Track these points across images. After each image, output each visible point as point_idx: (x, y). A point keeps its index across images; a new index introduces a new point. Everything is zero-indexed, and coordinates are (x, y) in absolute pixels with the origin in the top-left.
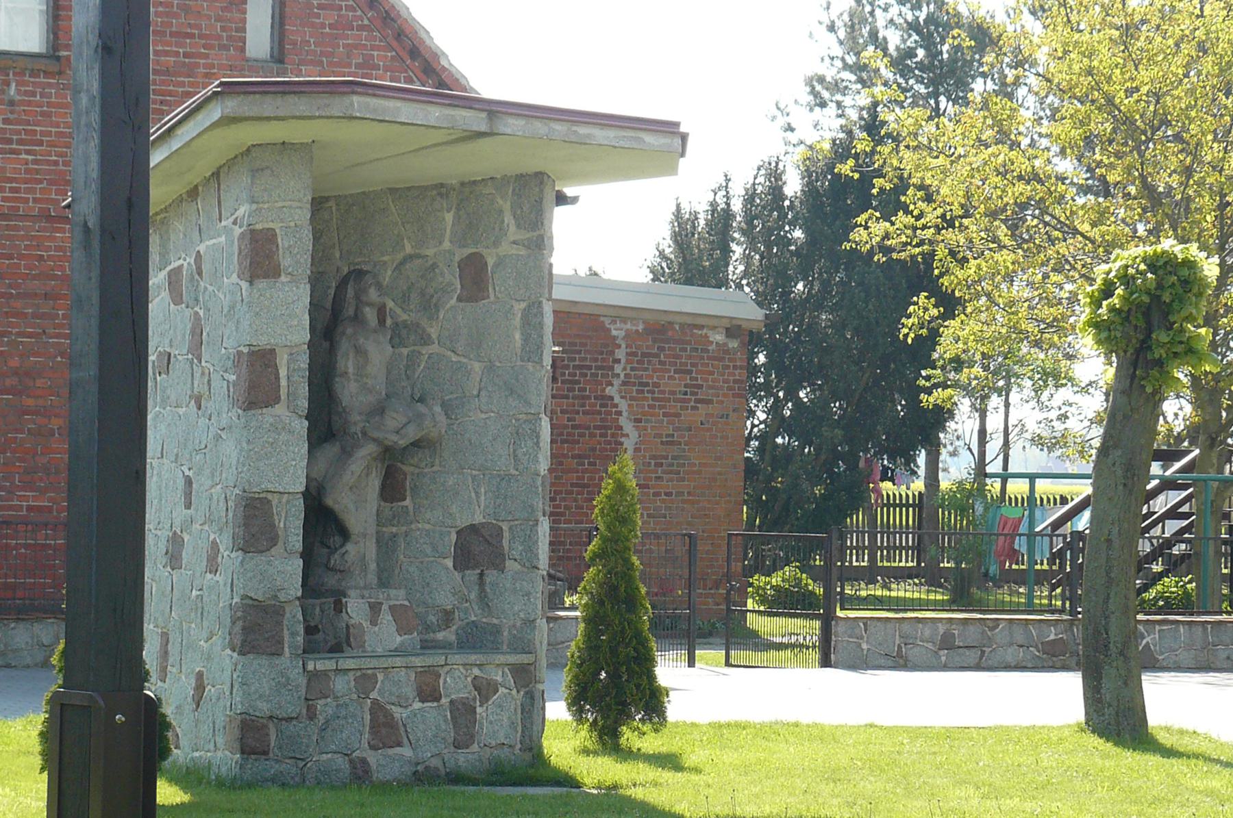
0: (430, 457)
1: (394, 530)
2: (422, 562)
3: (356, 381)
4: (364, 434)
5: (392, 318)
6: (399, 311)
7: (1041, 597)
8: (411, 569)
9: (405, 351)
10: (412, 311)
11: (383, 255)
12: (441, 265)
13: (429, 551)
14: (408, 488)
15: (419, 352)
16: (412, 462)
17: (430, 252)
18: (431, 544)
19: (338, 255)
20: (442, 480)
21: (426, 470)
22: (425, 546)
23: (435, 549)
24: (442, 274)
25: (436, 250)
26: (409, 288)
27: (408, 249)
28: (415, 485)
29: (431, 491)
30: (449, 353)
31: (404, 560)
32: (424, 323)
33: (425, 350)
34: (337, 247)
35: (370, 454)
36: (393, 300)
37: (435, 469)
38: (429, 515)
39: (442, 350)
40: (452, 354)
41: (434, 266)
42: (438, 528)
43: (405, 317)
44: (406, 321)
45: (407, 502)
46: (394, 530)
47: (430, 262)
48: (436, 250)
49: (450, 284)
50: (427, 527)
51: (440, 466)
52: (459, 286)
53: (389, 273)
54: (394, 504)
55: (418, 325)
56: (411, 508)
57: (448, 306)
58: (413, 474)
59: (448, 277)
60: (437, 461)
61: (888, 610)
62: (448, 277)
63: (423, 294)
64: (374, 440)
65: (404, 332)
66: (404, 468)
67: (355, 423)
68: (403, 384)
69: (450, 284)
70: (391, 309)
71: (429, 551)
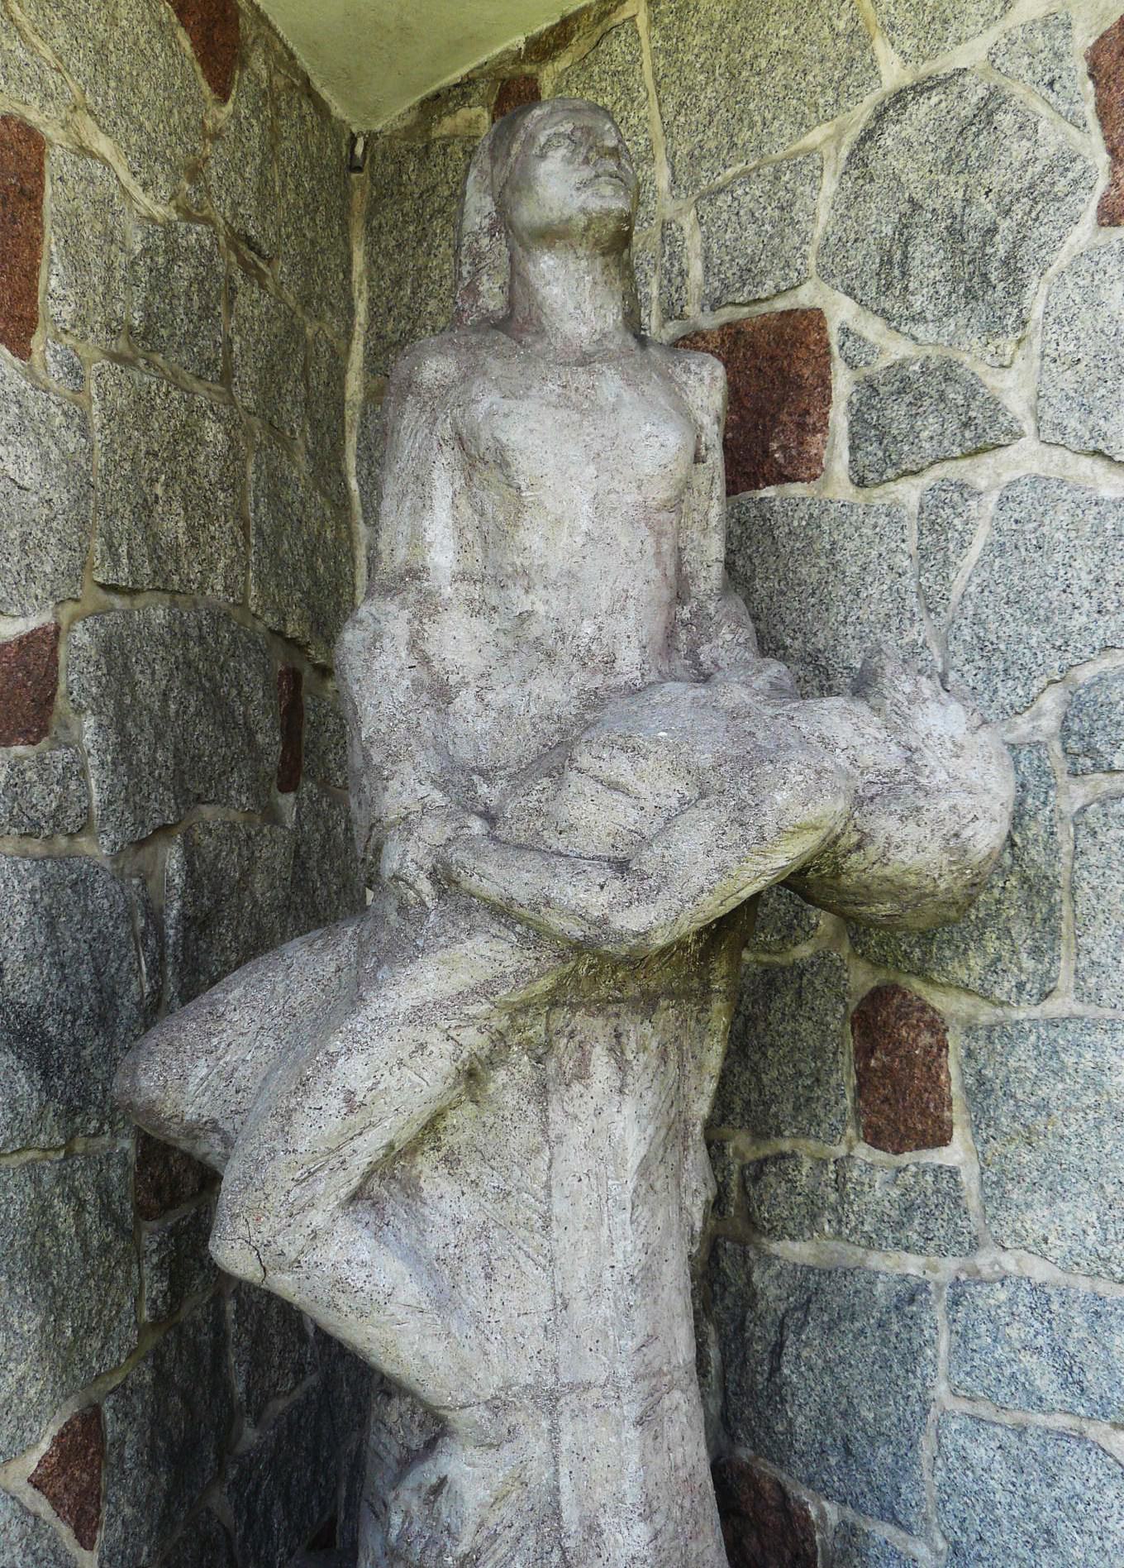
0: (1036, 952)
1: (913, 1265)
2: (1021, 1431)
3: (477, 609)
4: (444, 879)
5: (852, 365)
6: (872, 329)
7: (183, 449)
8: (979, 1454)
9: (909, 493)
10: (918, 318)
11: (803, 126)
12: (1018, 90)
13: (1045, 1381)
14: (955, 1089)
15: (962, 487)
16: (962, 974)
17: (969, 54)
18: (1057, 1351)
19: (663, 178)
20: (1087, 1063)
21: (1019, 1015)
22: (1028, 1360)
23: (1070, 1375)
24: (1026, 127)
25: (993, 35)
26: (903, 227)
27: (893, 72)
28: (981, 1081)
29: (1043, 1107)
30: (1086, 465)
31: (951, 1404)
32: (972, 357)
33: (985, 473)
34: (661, 156)
35: (485, 990)
36: (850, 292)
37: (1055, 1007)
38: (1037, 1219)
39: (1052, 462)
40: (1099, 467)
41: (992, 104)
42: (1084, 1285)
43: (897, 349)
44: (902, 365)
45: (956, 1153)
46: (913, 1265)
47: (976, 95)
48: (993, 35)
49: (1066, 159)
50: (1040, 1271)
51: (1083, 995)
52: (1102, 159)
53: (829, 185)
54: (907, 1158)
55: (948, 371)
56: (969, 1178)
57: (1061, 259)
58: (970, 1029)
59: (1053, 134)
60: (1065, 978)
61: (348, 272)
62: (1053, 134)
63: (955, 234)
64: (502, 912)
65: (897, 411)
66: (943, 1002)
67: (406, 823)
68: (912, 635)
69: (1066, 159)
70: (846, 332)
71: (1045, 1381)
